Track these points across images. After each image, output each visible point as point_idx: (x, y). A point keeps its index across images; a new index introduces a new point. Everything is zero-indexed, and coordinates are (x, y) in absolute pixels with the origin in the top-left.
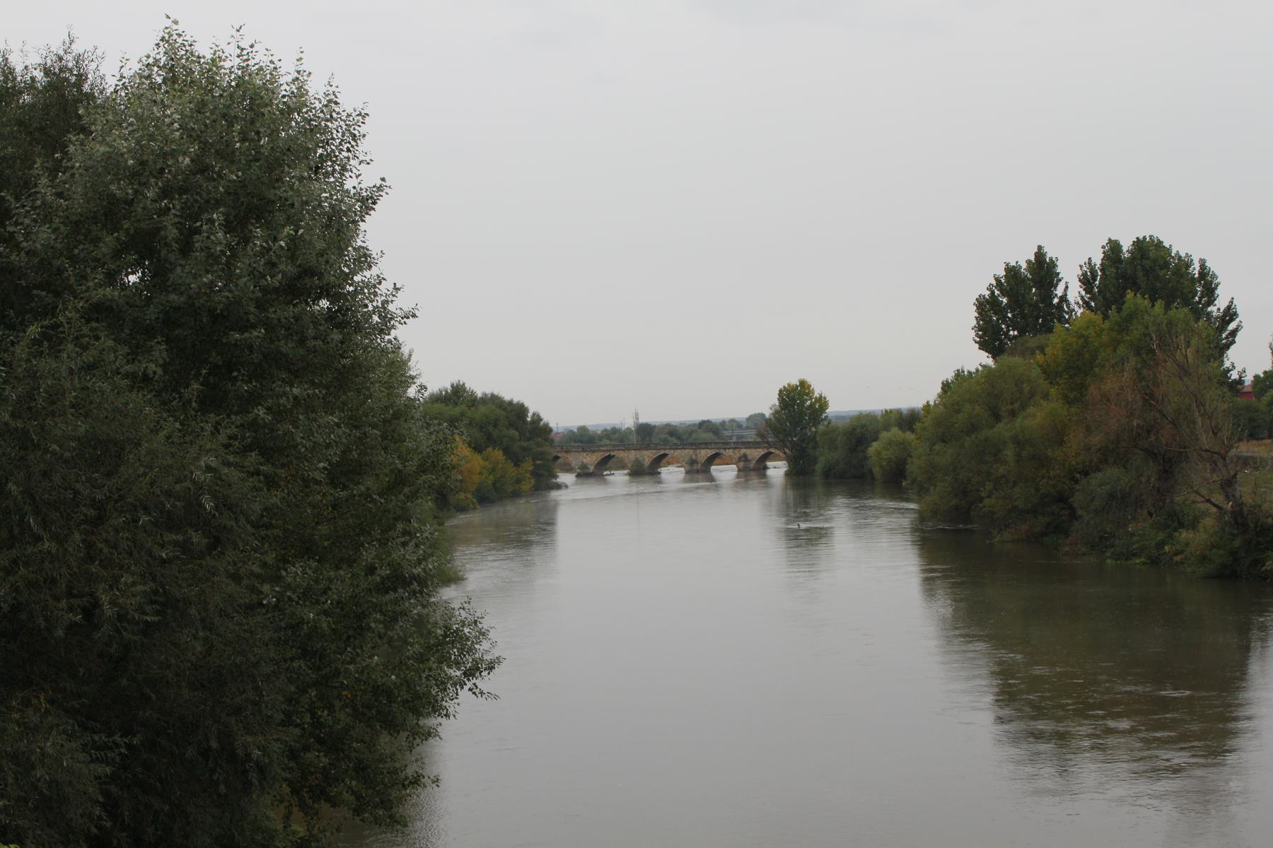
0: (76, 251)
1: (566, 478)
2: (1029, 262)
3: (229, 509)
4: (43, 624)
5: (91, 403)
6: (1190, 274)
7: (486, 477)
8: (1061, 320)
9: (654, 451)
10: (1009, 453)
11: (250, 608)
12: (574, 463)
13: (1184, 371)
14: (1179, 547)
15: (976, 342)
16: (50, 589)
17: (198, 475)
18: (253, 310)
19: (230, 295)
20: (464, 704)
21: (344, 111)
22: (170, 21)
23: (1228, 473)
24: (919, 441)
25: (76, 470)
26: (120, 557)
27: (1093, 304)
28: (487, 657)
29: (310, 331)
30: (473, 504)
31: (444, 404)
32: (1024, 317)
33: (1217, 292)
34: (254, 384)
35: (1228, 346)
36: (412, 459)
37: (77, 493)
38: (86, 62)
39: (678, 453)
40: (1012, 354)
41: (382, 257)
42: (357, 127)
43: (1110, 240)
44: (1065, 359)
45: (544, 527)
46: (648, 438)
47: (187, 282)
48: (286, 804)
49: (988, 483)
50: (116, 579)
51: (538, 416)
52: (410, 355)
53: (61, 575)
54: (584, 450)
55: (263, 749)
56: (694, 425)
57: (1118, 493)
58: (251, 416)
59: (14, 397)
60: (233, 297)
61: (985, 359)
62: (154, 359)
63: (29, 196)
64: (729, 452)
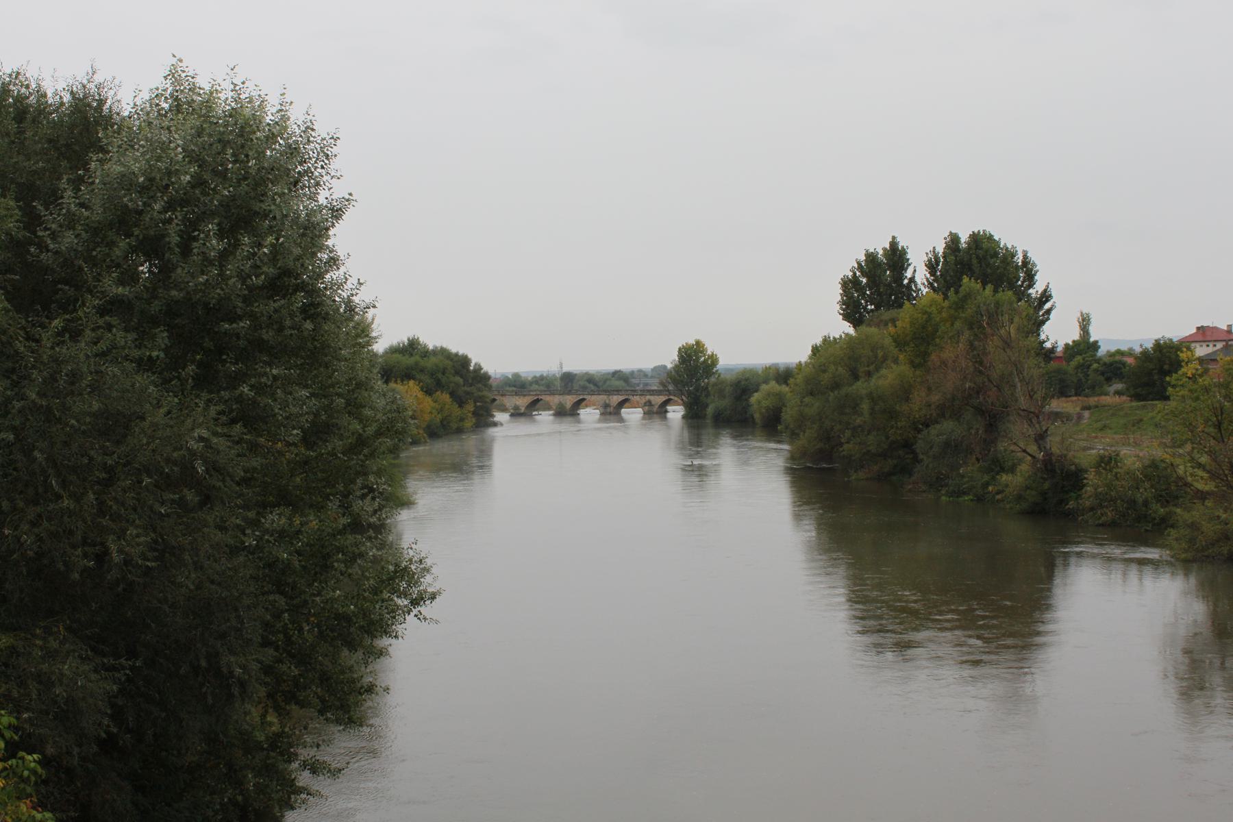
0: (94, 253)
1: (500, 417)
2: (884, 249)
3: (217, 471)
4: (63, 569)
5: (105, 384)
6: (1014, 262)
7: (435, 416)
8: (910, 298)
9: (575, 396)
10: (865, 406)
11: (234, 551)
12: (508, 404)
13: (1007, 344)
14: (1000, 488)
15: (840, 314)
16: (69, 539)
17: (193, 444)
18: (240, 304)
19: (222, 293)
20: (409, 626)
21: (319, 136)
22: (175, 59)
23: (1041, 429)
24: (792, 394)
25: (90, 439)
26: (127, 512)
27: (936, 285)
28: (430, 590)
29: (287, 322)
30: (424, 438)
31: (401, 355)
32: (880, 294)
33: (1036, 278)
34: (240, 365)
35: (1043, 322)
36: (371, 426)
37: (91, 459)
38: (106, 90)
39: (594, 398)
40: (869, 325)
41: (348, 258)
42: (330, 149)
43: (951, 232)
44: (912, 331)
45: (485, 452)
46: (570, 384)
47: (186, 280)
48: (263, 705)
49: (847, 431)
50: (124, 531)
51: (479, 365)
52: (373, 319)
53: (77, 527)
54: (516, 394)
55: (243, 667)
56: (608, 374)
57: (953, 442)
58: (237, 392)
59: (40, 380)
60: (224, 294)
61: (848, 328)
62: (157, 344)
63: (57, 206)
64: (637, 398)
